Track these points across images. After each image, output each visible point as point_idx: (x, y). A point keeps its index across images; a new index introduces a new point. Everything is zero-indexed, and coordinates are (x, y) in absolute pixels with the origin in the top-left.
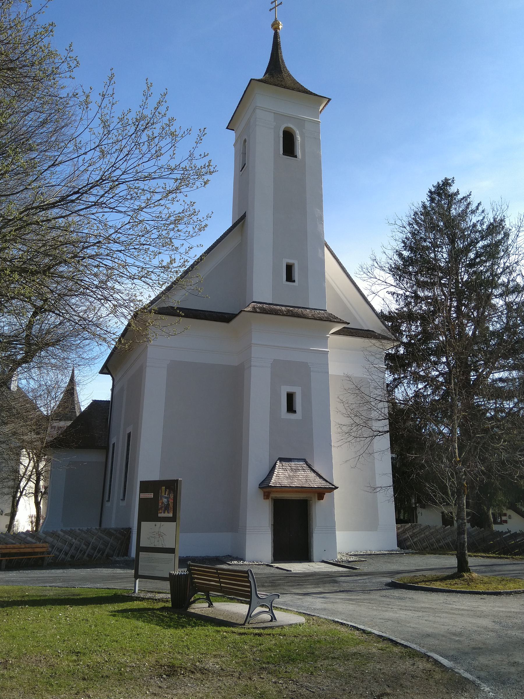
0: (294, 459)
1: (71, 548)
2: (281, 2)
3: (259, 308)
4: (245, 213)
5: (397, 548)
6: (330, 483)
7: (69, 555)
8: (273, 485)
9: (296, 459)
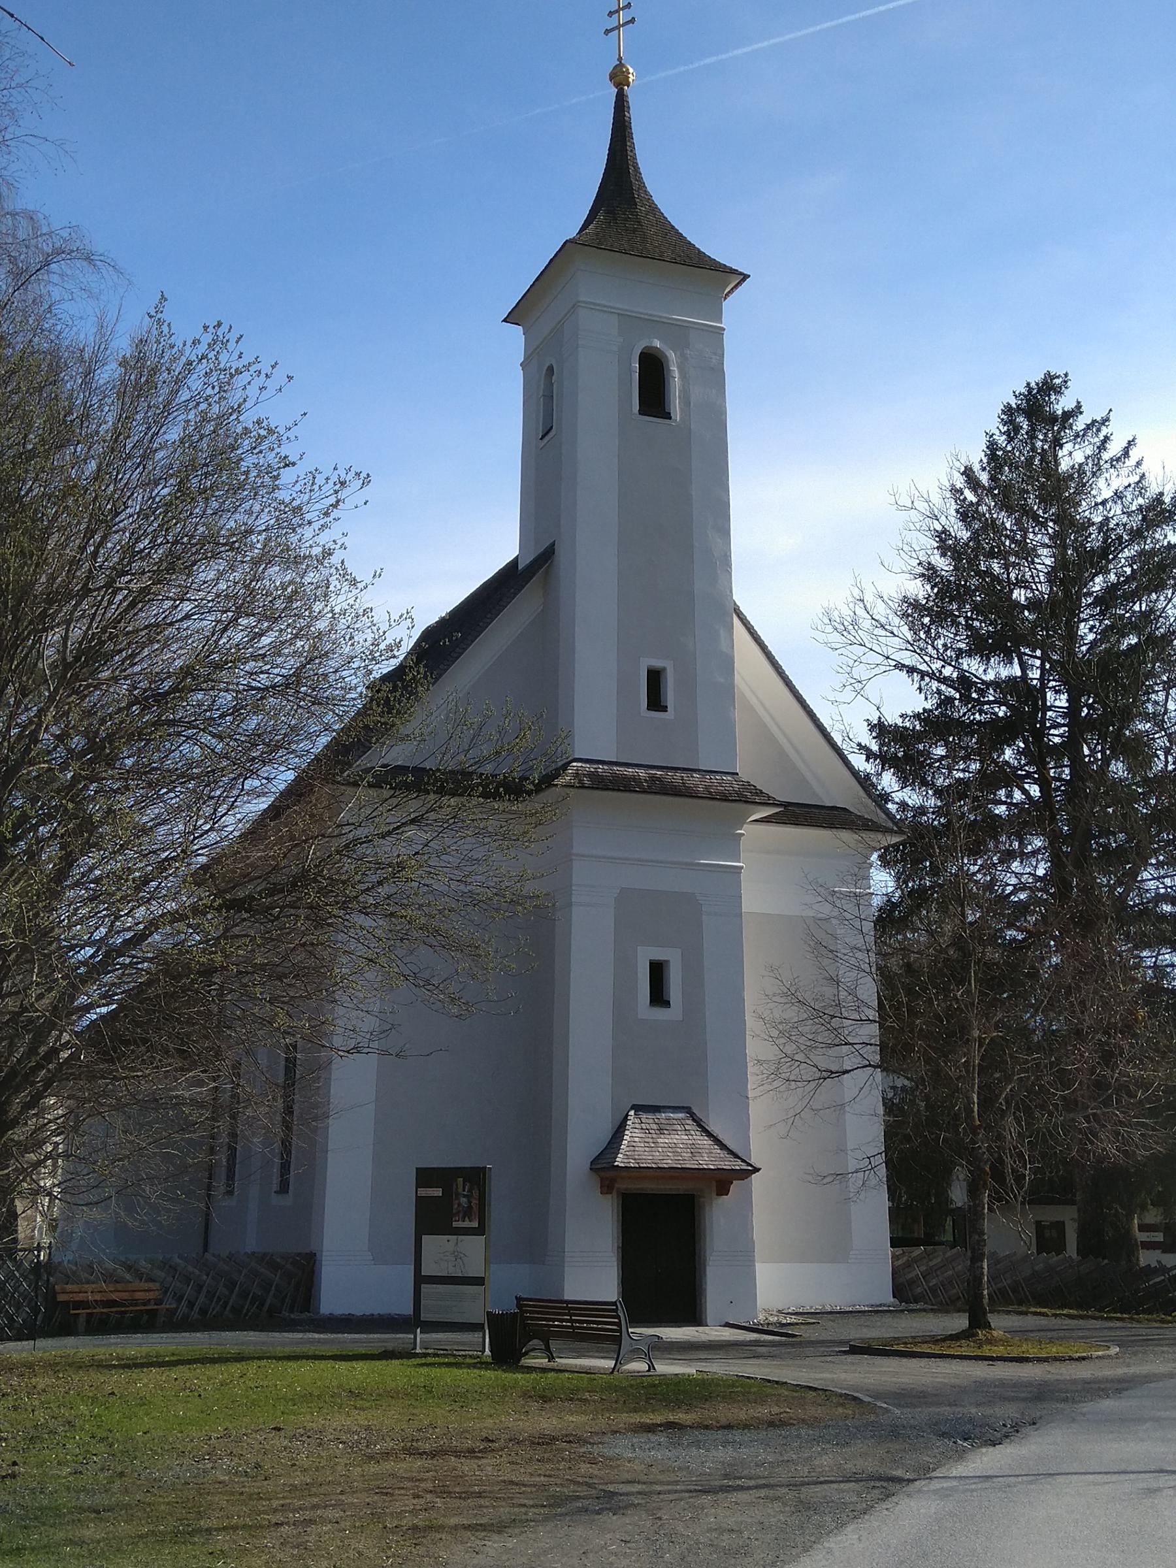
0: (664, 1107)
1: (199, 1292)
2: (634, 18)
3: (591, 775)
4: (553, 544)
5: (892, 1300)
6: (743, 1161)
7: (196, 1308)
8: (622, 1165)
9: (669, 1107)
